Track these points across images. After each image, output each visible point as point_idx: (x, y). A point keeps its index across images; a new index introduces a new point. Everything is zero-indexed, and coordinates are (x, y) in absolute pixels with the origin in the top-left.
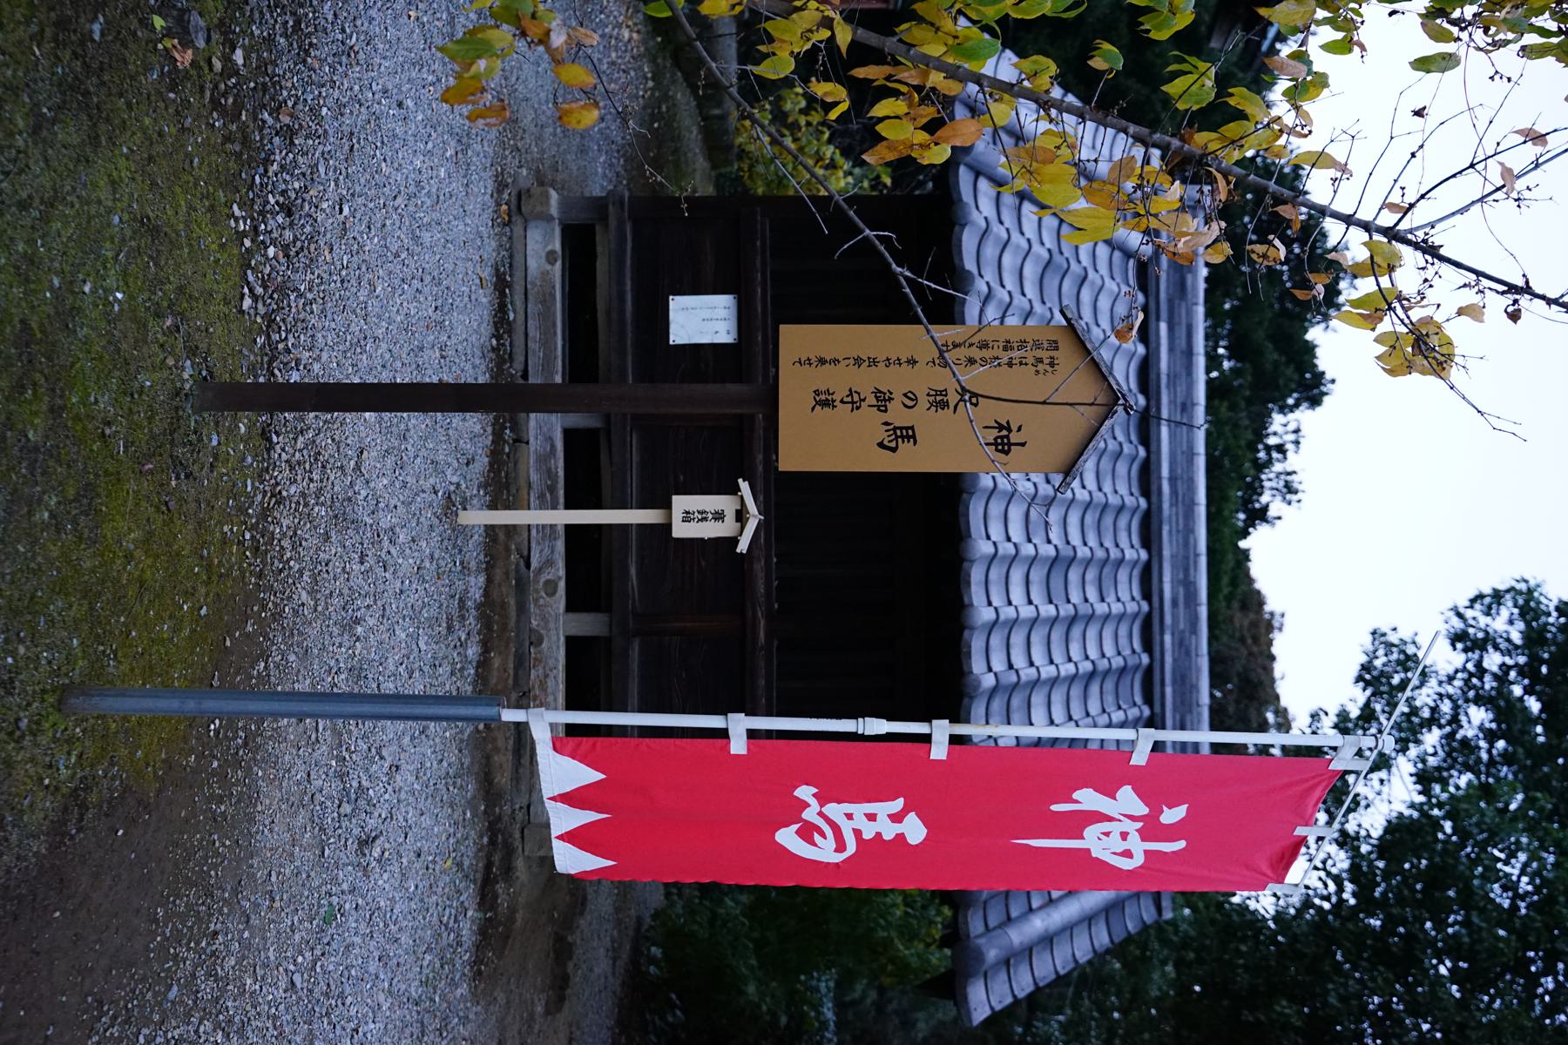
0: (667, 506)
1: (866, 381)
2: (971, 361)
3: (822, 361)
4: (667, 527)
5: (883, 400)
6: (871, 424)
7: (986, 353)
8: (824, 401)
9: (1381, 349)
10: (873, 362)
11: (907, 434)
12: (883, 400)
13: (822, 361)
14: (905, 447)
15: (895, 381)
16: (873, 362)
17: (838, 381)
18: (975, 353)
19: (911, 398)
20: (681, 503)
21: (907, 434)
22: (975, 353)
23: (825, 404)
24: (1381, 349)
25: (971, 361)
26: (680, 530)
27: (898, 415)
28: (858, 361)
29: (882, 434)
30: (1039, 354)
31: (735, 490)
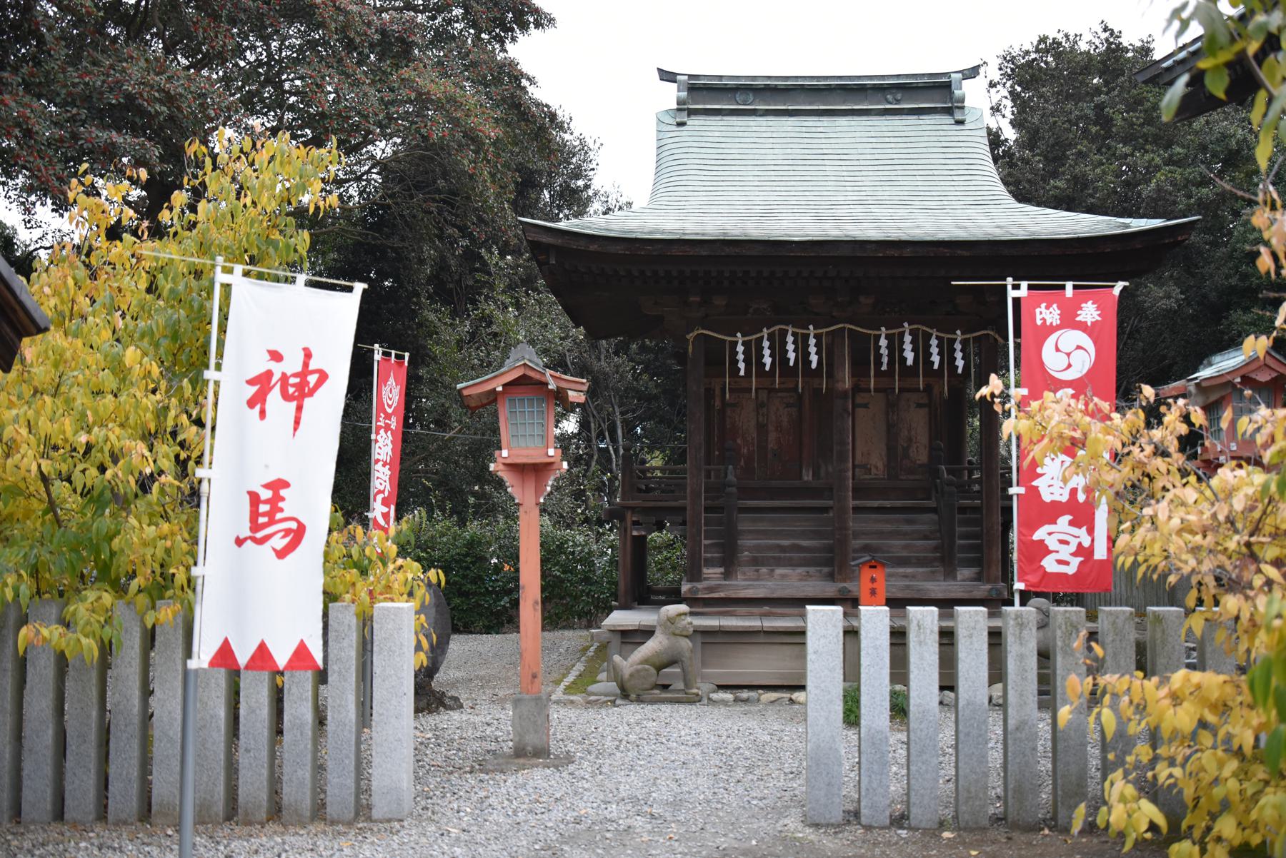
9: (281, 504)
24: (281, 504)
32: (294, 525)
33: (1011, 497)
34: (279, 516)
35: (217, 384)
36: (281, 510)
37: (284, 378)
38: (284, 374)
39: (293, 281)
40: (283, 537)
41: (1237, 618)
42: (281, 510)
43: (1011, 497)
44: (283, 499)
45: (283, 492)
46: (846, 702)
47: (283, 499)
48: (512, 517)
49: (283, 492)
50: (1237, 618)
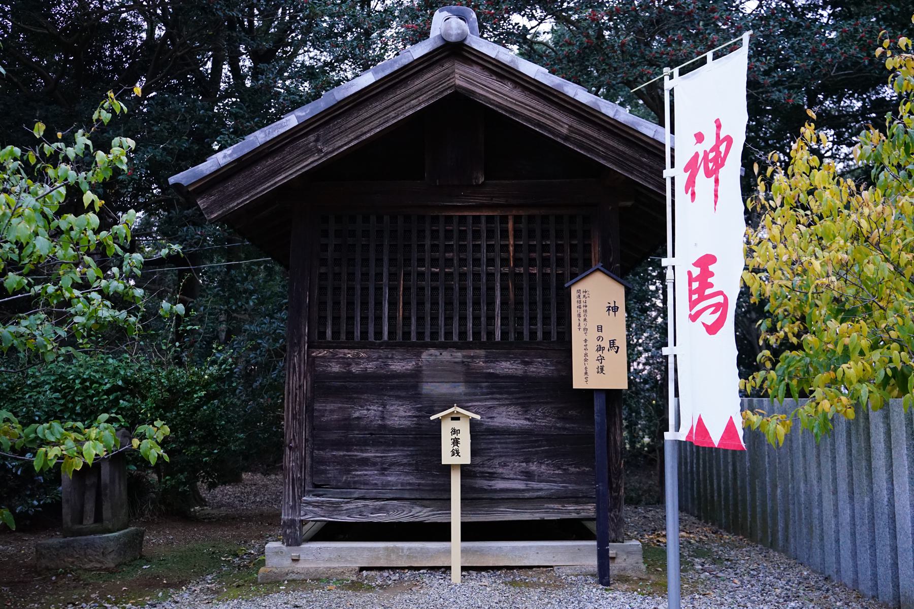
0: (448, 467)
1: (593, 355)
2: (585, 320)
3: (586, 373)
4: (463, 466)
5: (600, 348)
6: (609, 355)
7: (582, 314)
8: (601, 370)
9: (710, 280)
10: (586, 355)
11: (612, 343)
12: (600, 348)
13: (586, 373)
14: (617, 344)
15: (593, 345)
16: (586, 355)
17: (593, 365)
18: (582, 318)
19: (599, 338)
20: (447, 458)
21: (612, 343)
22: (582, 318)
23: (602, 369)
24: (710, 280)
25: (585, 320)
26: (465, 458)
27: (606, 344)
28: (586, 360)
29: (613, 351)
30: (582, 296)
31: (439, 421)
32: (720, 299)
33: (666, 357)
34: (708, 292)
35: (673, 179)
36: (711, 285)
37: (706, 154)
38: (705, 151)
39: (703, 62)
40: (713, 313)
41: (126, 237)
42: (711, 285)
43: (666, 357)
44: (712, 274)
45: (711, 268)
46: (417, 42)
47: (712, 274)
48: (759, 193)
49: (711, 268)
50: (126, 237)
